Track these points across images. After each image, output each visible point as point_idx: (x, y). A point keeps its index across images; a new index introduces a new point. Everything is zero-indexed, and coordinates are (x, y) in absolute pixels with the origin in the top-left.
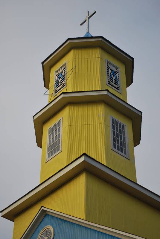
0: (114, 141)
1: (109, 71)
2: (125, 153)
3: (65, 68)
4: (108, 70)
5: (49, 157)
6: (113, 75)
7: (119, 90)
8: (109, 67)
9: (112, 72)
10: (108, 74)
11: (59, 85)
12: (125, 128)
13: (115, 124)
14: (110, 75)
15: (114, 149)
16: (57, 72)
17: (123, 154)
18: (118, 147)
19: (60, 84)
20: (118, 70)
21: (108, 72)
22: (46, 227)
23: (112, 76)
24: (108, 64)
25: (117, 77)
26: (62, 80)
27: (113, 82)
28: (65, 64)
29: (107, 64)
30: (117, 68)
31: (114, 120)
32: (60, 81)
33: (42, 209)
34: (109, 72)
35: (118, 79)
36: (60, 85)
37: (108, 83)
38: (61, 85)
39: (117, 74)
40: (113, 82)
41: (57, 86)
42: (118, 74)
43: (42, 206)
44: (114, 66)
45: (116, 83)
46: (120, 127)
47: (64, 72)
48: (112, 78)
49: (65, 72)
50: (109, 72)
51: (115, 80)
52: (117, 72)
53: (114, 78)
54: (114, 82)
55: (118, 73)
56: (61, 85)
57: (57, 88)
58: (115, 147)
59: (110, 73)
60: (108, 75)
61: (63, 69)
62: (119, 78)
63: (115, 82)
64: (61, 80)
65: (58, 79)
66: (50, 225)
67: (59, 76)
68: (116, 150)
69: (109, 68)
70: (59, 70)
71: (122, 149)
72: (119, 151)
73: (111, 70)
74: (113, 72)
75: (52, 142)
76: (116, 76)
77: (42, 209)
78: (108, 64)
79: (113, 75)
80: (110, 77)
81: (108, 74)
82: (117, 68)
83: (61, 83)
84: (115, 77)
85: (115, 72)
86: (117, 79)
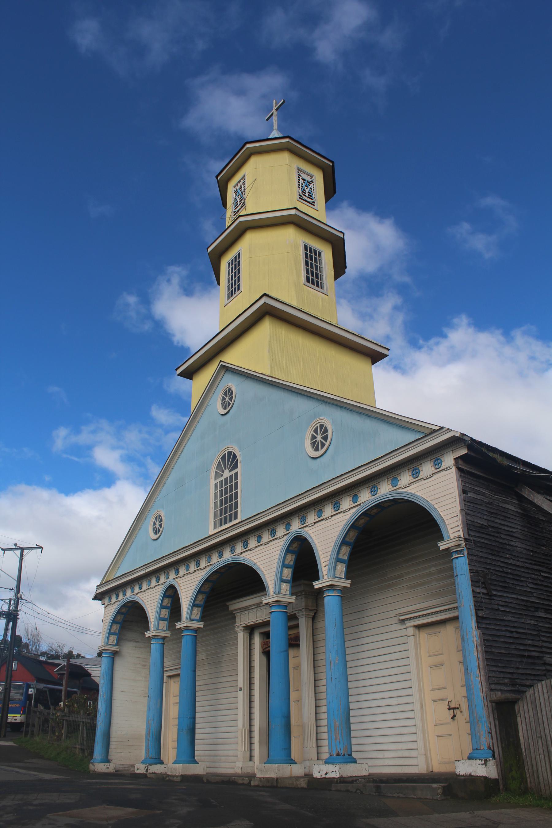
3: (244, 182)
6: (306, 186)
7: (314, 205)
8: (300, 175)
9: (304, 183)
10: (299, 185)
11: (237, 204)
12: (322, 254)
14: (302, 187)
15: (308, 284)
16: (235, 187)
17: (319, 289)
18: (313, 280)
19: (239, 203)
21: (299, 182)
23: (305, 187)
24: (299, 172)
25: (311, 189)
26: (241, 198)
27: (305, 196)
28: (244, 176)
29: (298, 172)
30: (312, 177)
32: (238, 199)
33: (221, 365)
36: (238, 205)
37: (300, 198)
40: (305, 196)
41: (236, 207)
42: (313, 185)
45: (310, 197)
48: (305, 190)
49: (244, 187)
51: (308, 192)
52: (311, 181)
54: (307, 196)
55: (313, 182)
57: (235, 209)
58: (308, 281)
59: (302, 184)
60: (299, 188)
63: (309, 195)
64: (240, 199)
65: (236, 196)
68: (310, 285)
70: (237, 184)
74: (306, 182)
76: (310, 187)
78: (299, 172)
79: (306, 186)
80: (302, 189)
81: (299, 185)
83: (240, 202)
84: (309, 189)
85: (308, 182)
86: (312, 192)
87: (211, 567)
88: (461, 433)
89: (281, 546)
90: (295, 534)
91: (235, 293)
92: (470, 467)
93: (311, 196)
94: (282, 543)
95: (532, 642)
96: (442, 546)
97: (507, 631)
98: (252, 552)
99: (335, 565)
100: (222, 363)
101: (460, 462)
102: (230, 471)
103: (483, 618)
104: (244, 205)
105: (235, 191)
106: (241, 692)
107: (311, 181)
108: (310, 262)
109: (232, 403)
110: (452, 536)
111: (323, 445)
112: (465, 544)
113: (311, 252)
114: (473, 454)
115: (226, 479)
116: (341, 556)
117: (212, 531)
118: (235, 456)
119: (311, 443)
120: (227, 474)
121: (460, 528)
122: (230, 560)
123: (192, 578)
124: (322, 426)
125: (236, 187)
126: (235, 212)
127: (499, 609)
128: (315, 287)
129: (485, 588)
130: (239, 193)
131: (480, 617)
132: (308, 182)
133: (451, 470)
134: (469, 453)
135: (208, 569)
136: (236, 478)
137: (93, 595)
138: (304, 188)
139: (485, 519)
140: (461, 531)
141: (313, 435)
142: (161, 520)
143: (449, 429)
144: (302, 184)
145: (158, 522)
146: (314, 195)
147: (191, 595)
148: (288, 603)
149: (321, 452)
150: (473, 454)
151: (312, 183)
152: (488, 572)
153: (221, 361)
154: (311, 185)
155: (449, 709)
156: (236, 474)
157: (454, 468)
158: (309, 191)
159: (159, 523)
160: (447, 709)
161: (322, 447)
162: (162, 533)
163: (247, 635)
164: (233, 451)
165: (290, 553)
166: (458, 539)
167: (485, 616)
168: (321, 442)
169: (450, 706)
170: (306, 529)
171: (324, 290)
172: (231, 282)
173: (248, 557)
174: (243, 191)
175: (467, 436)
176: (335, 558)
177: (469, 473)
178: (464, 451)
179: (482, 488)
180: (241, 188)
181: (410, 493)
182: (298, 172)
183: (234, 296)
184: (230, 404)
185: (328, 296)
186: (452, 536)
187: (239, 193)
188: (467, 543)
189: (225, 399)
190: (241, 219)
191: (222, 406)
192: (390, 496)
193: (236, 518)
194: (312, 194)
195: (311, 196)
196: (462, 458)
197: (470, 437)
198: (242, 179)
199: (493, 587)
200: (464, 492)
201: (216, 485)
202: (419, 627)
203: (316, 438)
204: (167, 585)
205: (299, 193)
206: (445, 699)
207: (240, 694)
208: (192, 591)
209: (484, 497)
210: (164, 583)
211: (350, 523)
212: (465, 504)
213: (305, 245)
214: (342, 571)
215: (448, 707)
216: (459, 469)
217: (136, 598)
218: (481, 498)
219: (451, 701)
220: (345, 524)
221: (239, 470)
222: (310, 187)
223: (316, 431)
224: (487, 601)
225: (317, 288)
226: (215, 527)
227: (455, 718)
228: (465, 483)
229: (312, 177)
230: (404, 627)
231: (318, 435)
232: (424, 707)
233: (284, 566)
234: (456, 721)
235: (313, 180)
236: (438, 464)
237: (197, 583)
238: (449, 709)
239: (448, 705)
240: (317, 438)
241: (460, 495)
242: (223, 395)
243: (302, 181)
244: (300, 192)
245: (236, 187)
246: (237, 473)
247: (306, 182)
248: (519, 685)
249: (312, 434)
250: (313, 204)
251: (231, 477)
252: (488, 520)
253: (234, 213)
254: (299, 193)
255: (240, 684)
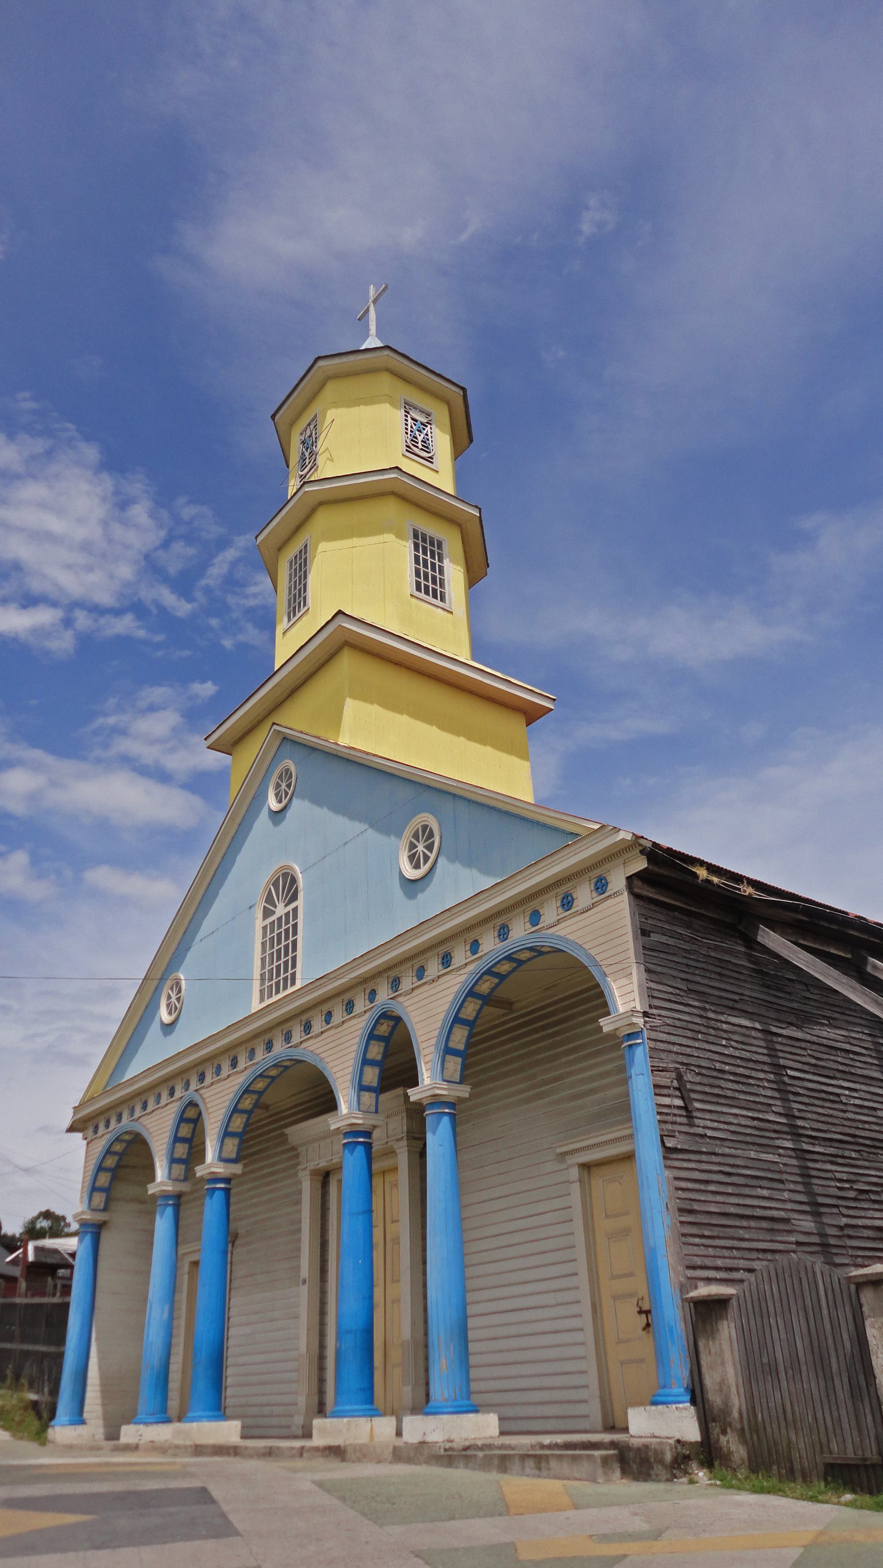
0: (415, 563)
1: (409, 423)
2: (443, 599)
3: (316, 425)
4: (406, 420)
5: (289, 620)
6: (419, 431)
7: (432, 463)
8: (408, 413)
9: (415, 425)
10: (407, 429)
11: (305, 463)
12: (445, 546)
13: (420, 539)
14: (412, 431)
15: (417, 594)
16: (301, 434)
17: (438, 602)
18: (427, 587)
19: (307, 461)
20: (430, 418)
21: (406, 425)
22: (283, 763)
23: (417, 433)
24: (407, 406)
25: (427, 435)
26: (312, 452)
27: (417, 447)
28: (316, 416)
29: (405, 407)
30: (428, 415)
31: (418, 531)
32: (307, 454)
33: (274, 729)
34: (409, 425)
35: (430, 439)
36: (307, 464)
37: (407, 450)
38: (309, 463)
39: (428, 429)
40: (417, 447)
41: (303, 467)
42: (431, 428)
43: (274, 724)
44: (422, 411)
45: (426, 448)
46: (432, 544)
47: (314, 434)
48: (416, 438)
49: (316, 434)
50: (409, 425)
51: (422, 441)
52: (428, 423)
53: (420, 439)
54: (420, 447)
55: (430, 424)
56: (309, 463)
57: (302, 471)
58: (418, 589)
59: (412, 427)
60: (407, 433)
61: (312, 427)
62: (432, 437)
63: (423, 445)
64: (310, 453)
65: (304, 449)
66: (290, 759)
67: (306, 444)
68: (422, 595)
69: (409, 416)
70: (306, 430)
71: (435, 591)
72: (429, 596)
73: (413, 419)
74: (418, 424)
75: (295, 594)
76: (425, 432)
77: (274, 729)
78: (407, 406)
79: (418, 430)
80: (411, 435)
81: (407, 429)
82: (428, 415)
83: (309, 459)
84: (422, 436)
85: (422, 424)
86: (428, 440)
87: (254, 1068)
88: (634, 834)
89: (361, 1031)
90: (383, 1008)
91: (299, 611)
92: (654, 891)
93: (427, 448)
94: (363, 1024)
95: (769, 1192)
96: (607, 1024)
97: (721, 1172)
98: (317, 1040)
99: (443, 1061)
100: (275, 727)
101: (637, 883)
102: (286, 906)
103: (675, 1150)
104: (315, 464)
105: (303, 442)
106: (306, 1286)
107: (428, 423)
108: (423, 558)
109: (290, 792)
110: (621, 1009)
111: (426, 858)
112: (644, 1022)
113: (424, 540)
114: (656, 869)
115: (280, 919)
116: (452, 1045)
117: (256, 1006)
118: (294, 880)
119: (408, 856)
120: (281, 910)
121: (636, 995)
122: (283, 1055)
123: (223, 1088)
124: (425, 827)
125: (304, 435)
126: (302, 475)
127: (706, 1135)
128: (430, 599)
129: (683, 1098)
130: (308, 444)
131: (669, 1148)
132: (422, 424)
133: (621, 896)
134: (651, 867)
135: (248, 1072)
136: (295, 917)
137: (67, 1122)
138: (415, 434)
139: (682, 979)
140: (637, 1000)
141: (411, 843)
142: (180, 991)
143: (615, 828)
144: (412, 427)
145: (175, 993)
146: (432, 445)
147: (221, 1117)
148: (372, 1127)
149: (424, 869)
150: (656, 869)
151: (429, 426)
152: (686, 1069)
153: (274, 724)
154: (427, 429)
155: (641, 1312)
156: (295, 910)
157: (626, 894)
158: (424, 438)
159: (176, 995)
160: (637, 1315)
161: (425, 863)
162: (180, 1012)
163: (318, 1185)
164: (291, 872)
165: (375, 1040)
166: (631, 1013)
167: (679, 1147)
168: (424, 853)
169: (640, 1308)
170: (401, 999)
171: (445, 603)
172: (293, 593)
173: (311, 1049)
174: (314, 440)
175: (646, 839)
176: (443, 1048)
177: (651, 901)
178: (641, 864)
179: (677, 925)
180: (310, 436)
181: (558, 936)
182: (405, 407)
183: (298, 615)
184: (288, 793)
185: (452, 613)
186: (621, 1009)
187: (308, 444)
188: (647, 1019)
189: (281, 786)
190: (307, 488)
191: (277, 798)
192: (527, 942)
193: (293, 983)
194: (429, 444)
195: (427, 448)
196: (639, 875)
197: (650, 841)
198: (312, 420)
199: (693, 1096)
200: (645, 933)
201: (264, 928)
202: (667, 1203)
203: (417, 847)
204: (186, 1101)
205: (406, 442)
206: (632, 1295)
207: (304, 1289)
208: (224, 1111)
209: (682, 942)
210: (181, 1098)
211: (466, 988)
212: (644, 954)
213: (413, 529)
214: (455, 1070)
215: (638, 1309)
216: (635, 896)
217: (297, 1054)
218: (675, 942)
219: (642, 1299)
220: (458, 990)
221: (300, 903)
222: (425, 432)
223: (416, 836)
224: (684, 1120)
225: (434, 601)
226: (262, 1000)
227: (651, 1329)
228: (646, 919)
229: (429, 416)
230: (563, 1166)
231: (419, 842)
232: (598, 1310)
233: (366, 1062)
234: (651, 1334)
235: (430, 421)
236: (602, 887)
237: (231, 1096)
238: (641, 1312)
239: (637, 1306)
240: (417, 847)
241: (635, 938)
242: (277, 779)
243: (412, 421)
244: (408, 441)
245: (304, 435)
246: (296, 908)
247: (418, 424)
248: (744, 1270)
249: (410, 841)
250: (430, 460)
251: (287, 914)
252: (687, 980)
253: (300, 477)
254: (406, 442)
255: (305, 1272)
